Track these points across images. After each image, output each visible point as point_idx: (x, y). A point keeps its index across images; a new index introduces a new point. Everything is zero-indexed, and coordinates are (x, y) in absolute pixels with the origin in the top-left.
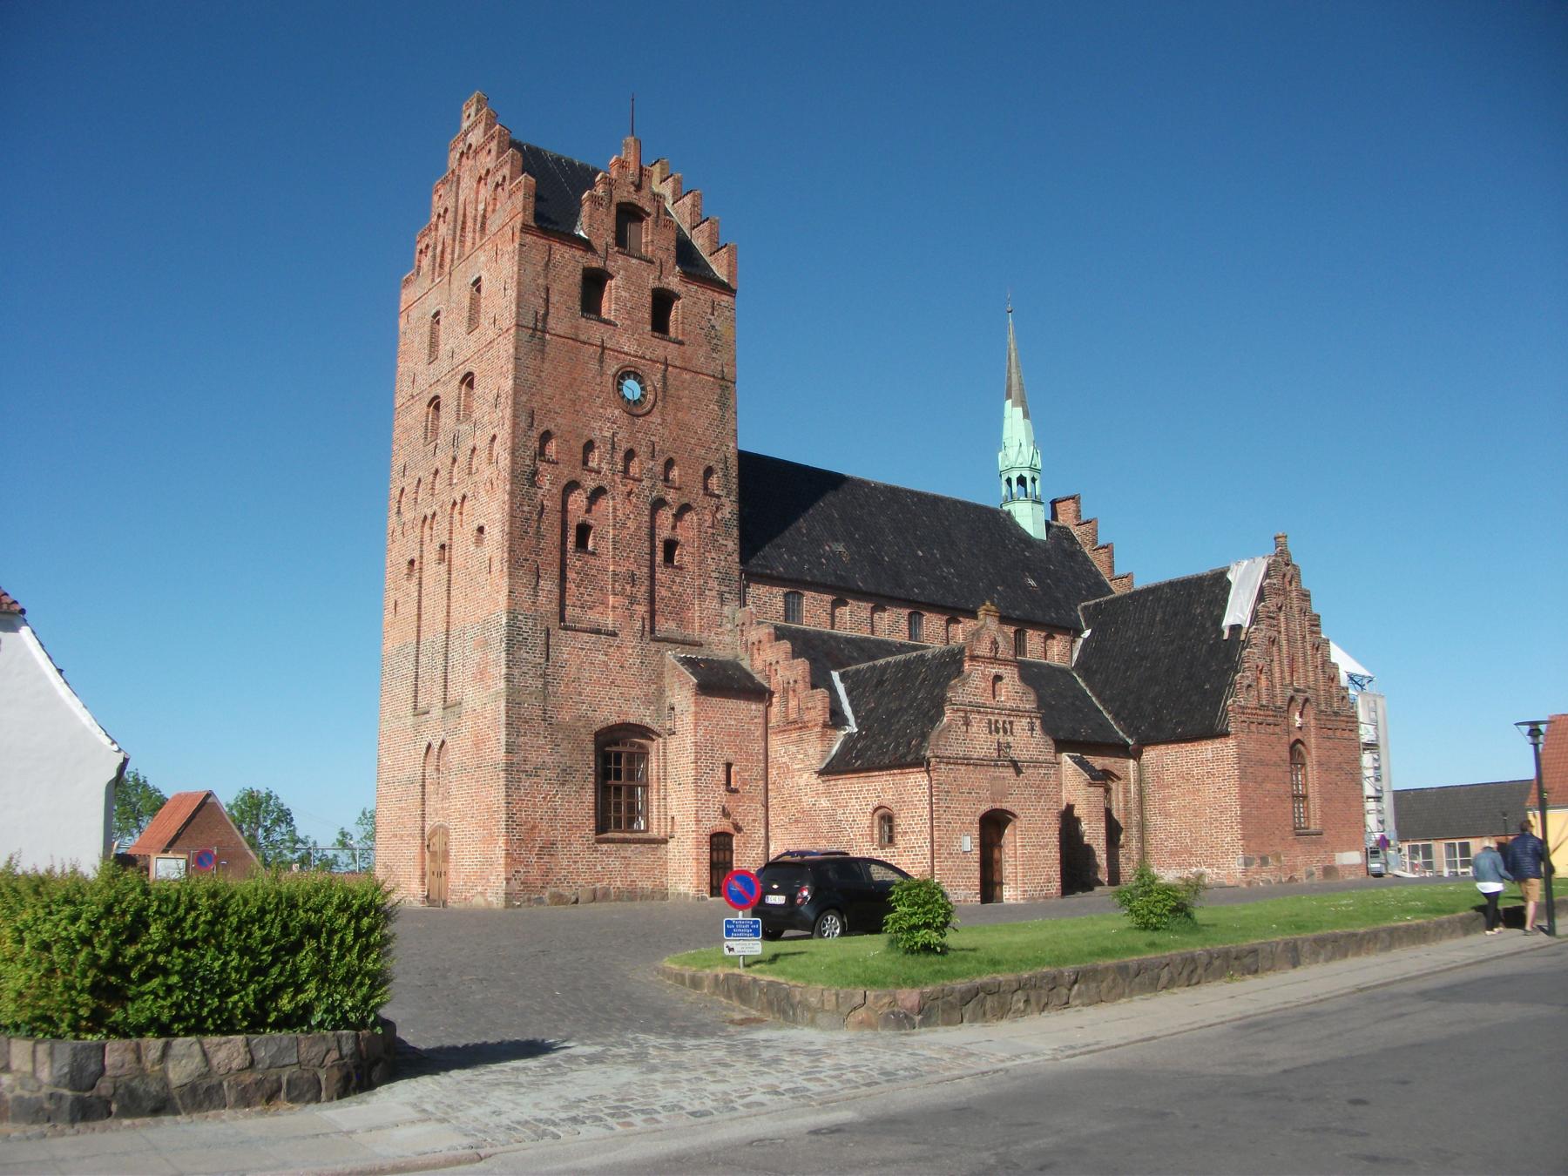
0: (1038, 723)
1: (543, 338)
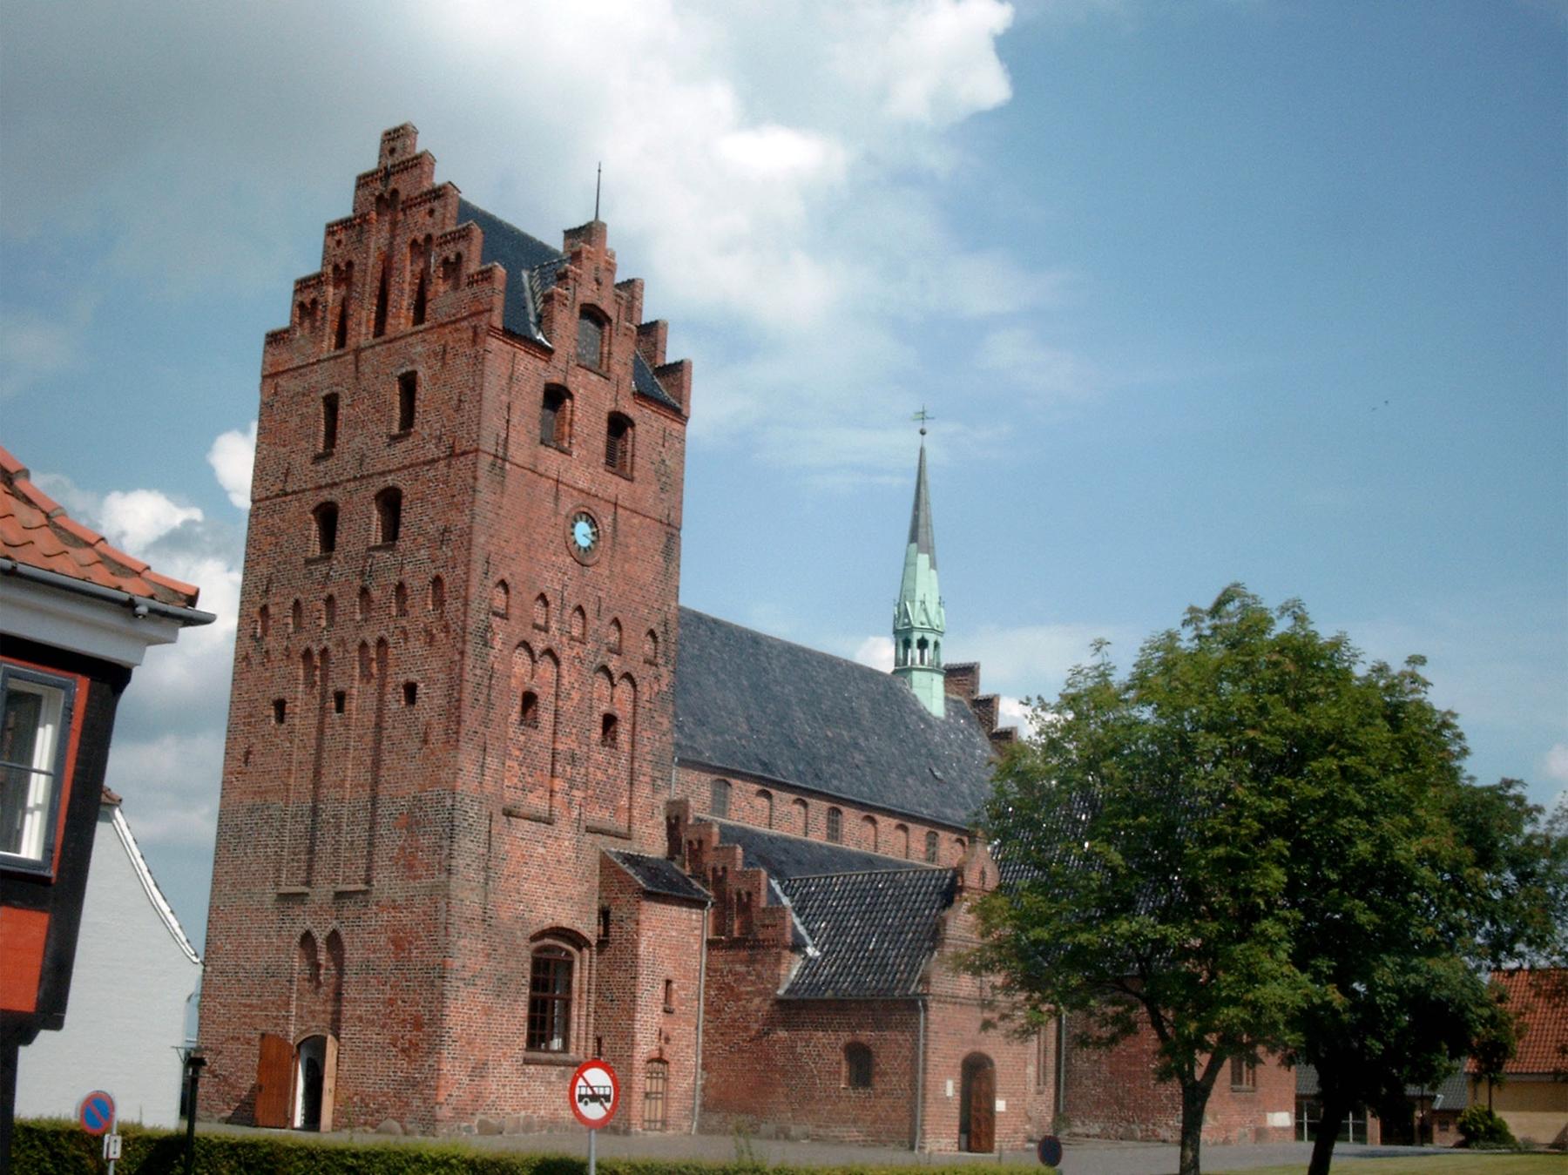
1: (502, 468)
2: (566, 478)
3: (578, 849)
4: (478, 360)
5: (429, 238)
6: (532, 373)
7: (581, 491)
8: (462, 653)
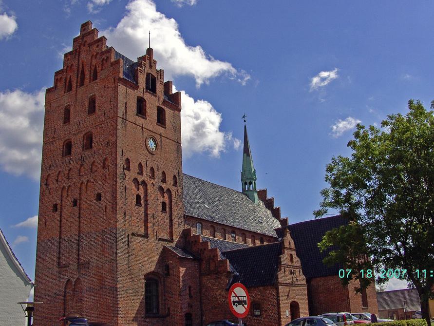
0: (301, 270)
1: (125, 122)
2: (145, 126)
3: (157, 246)
4: (116, 88)
5: (97, 53)
6: (134, 94)
7: (150, 131)
8: (116, 181)
